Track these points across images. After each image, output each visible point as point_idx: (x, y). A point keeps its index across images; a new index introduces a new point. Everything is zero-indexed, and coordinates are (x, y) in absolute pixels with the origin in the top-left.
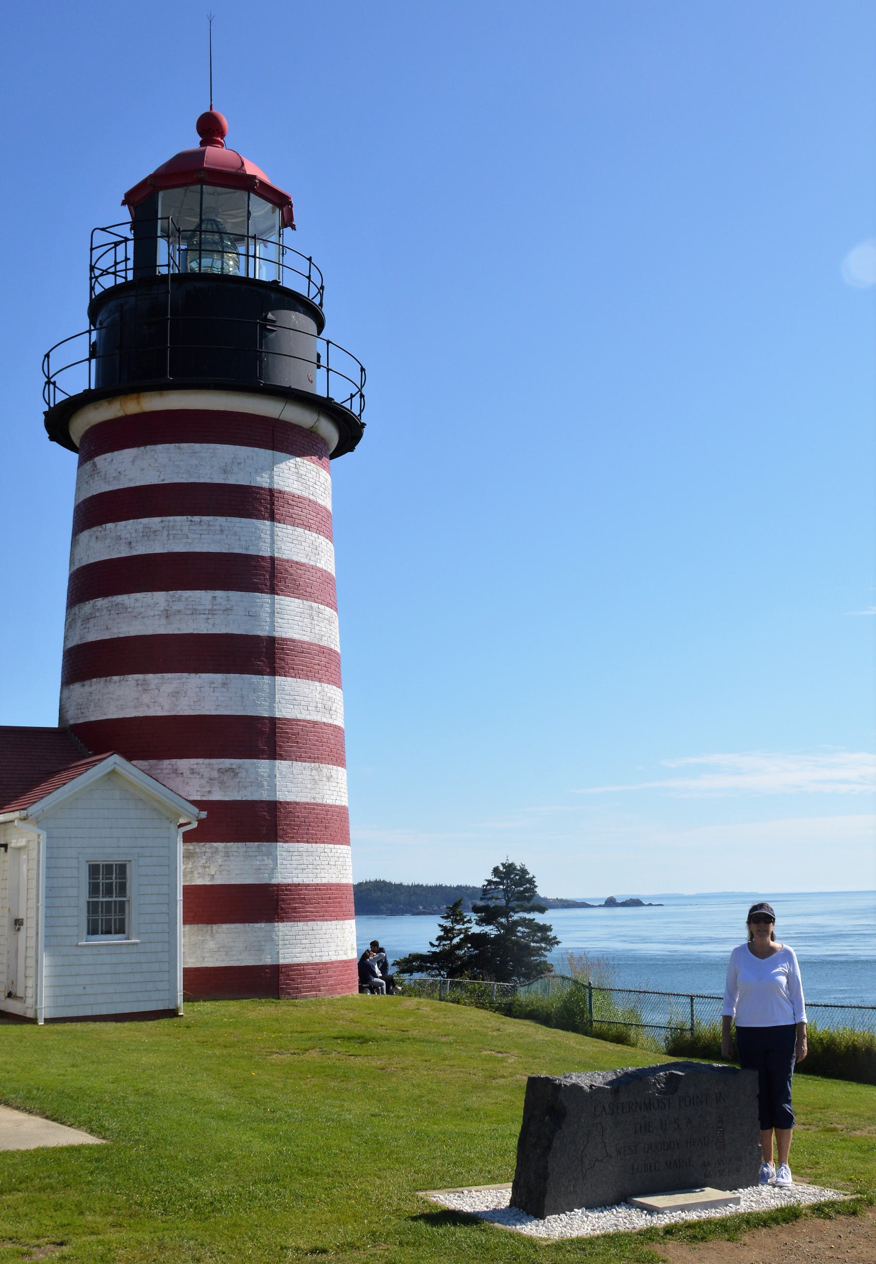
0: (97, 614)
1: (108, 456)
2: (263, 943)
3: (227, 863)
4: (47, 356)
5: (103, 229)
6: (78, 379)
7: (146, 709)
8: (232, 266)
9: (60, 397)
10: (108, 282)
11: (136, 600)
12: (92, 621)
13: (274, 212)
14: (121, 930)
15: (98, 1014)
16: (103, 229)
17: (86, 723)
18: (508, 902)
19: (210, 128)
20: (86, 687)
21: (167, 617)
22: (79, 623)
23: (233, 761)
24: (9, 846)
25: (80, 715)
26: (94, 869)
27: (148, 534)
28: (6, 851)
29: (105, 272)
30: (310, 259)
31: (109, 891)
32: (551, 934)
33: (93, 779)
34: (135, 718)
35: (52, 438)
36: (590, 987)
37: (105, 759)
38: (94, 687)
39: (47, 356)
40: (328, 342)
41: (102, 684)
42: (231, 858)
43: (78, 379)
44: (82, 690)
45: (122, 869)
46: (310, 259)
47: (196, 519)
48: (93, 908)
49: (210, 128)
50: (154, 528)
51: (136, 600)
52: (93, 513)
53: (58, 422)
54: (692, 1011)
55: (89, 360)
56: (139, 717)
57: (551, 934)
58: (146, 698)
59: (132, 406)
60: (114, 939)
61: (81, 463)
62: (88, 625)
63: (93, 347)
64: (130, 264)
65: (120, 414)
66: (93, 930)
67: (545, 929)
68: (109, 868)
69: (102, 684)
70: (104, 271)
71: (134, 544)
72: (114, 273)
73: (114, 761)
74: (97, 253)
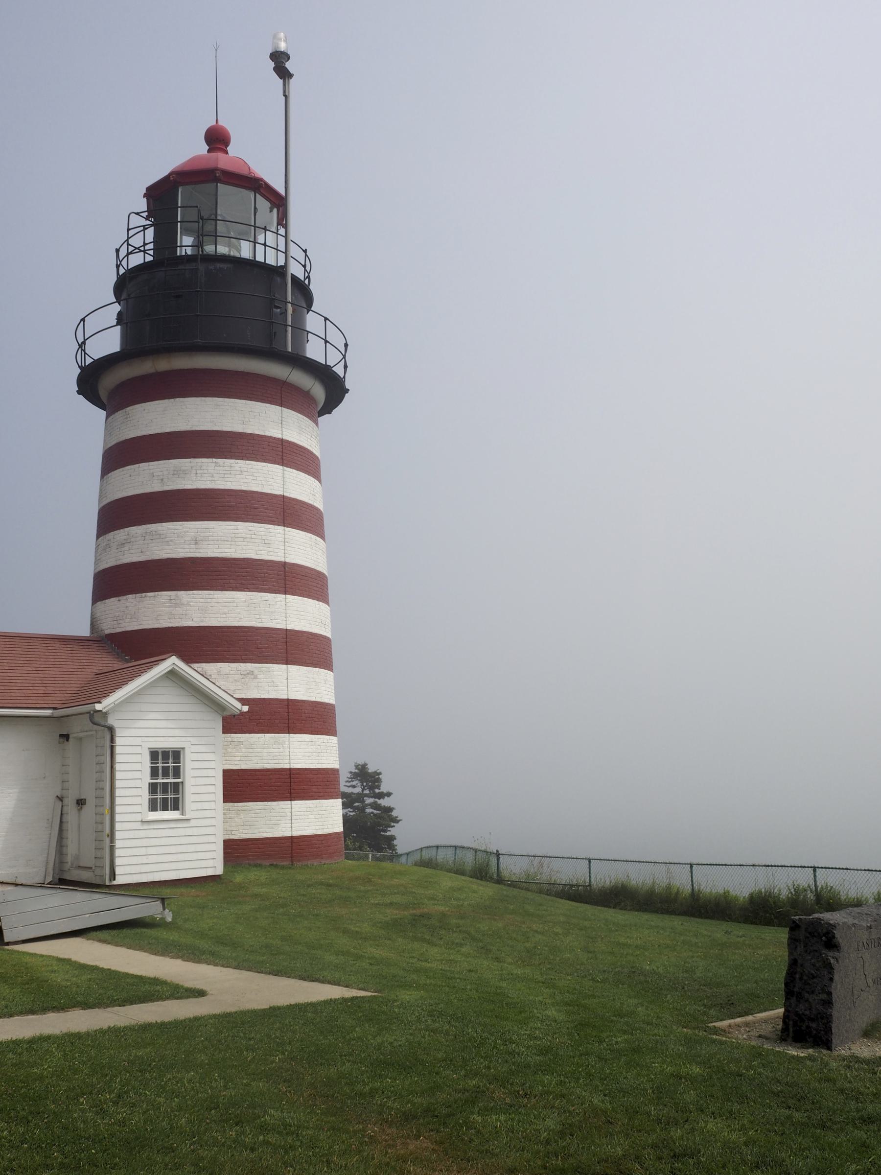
0: (133, 540)
1: (131, 408)
4: (83, 320)
5: (137, 214)
6: (108, 342)
8: (245, 251)
9: (89, 361)
10: (136, 260)
12: (127, 547)
13: (271, 211)
14: (176, 808)
16: (137, 214)
17: (122, 632)
18: (363, 790)
19: (217, 139)
20: (122, 602)
24: (71, 736)
25: (116, 626)
26: (154, 755)
27: (177, 472)
28: (68, 740)
29: (138, 250)
30: (305, 251)
31: (166, 773)
32: (394, 814)
36: (498, 855)
39: (83, 320)
40: (326, 319)
43: (108, 342)
46: (305, 251)
48: (153, 788)
49: (217, 139)
52: (120, 455)
53: (92, 381)
54: (815, 876)
55: (85, 340)
57: (394, 814)
59: (164, 364)
61: (107, 417)
62: (123, 549)
63: (120, 314)
64: (151, 246)
65: (152, 371)
66: (153, 807)
67: (390, 809)
68: (166, 754)
69: (138, 599)
70: (136, 248)
71: (165, 480)
72: (145, 251)
73: (173, 662)
74: (131, 233)
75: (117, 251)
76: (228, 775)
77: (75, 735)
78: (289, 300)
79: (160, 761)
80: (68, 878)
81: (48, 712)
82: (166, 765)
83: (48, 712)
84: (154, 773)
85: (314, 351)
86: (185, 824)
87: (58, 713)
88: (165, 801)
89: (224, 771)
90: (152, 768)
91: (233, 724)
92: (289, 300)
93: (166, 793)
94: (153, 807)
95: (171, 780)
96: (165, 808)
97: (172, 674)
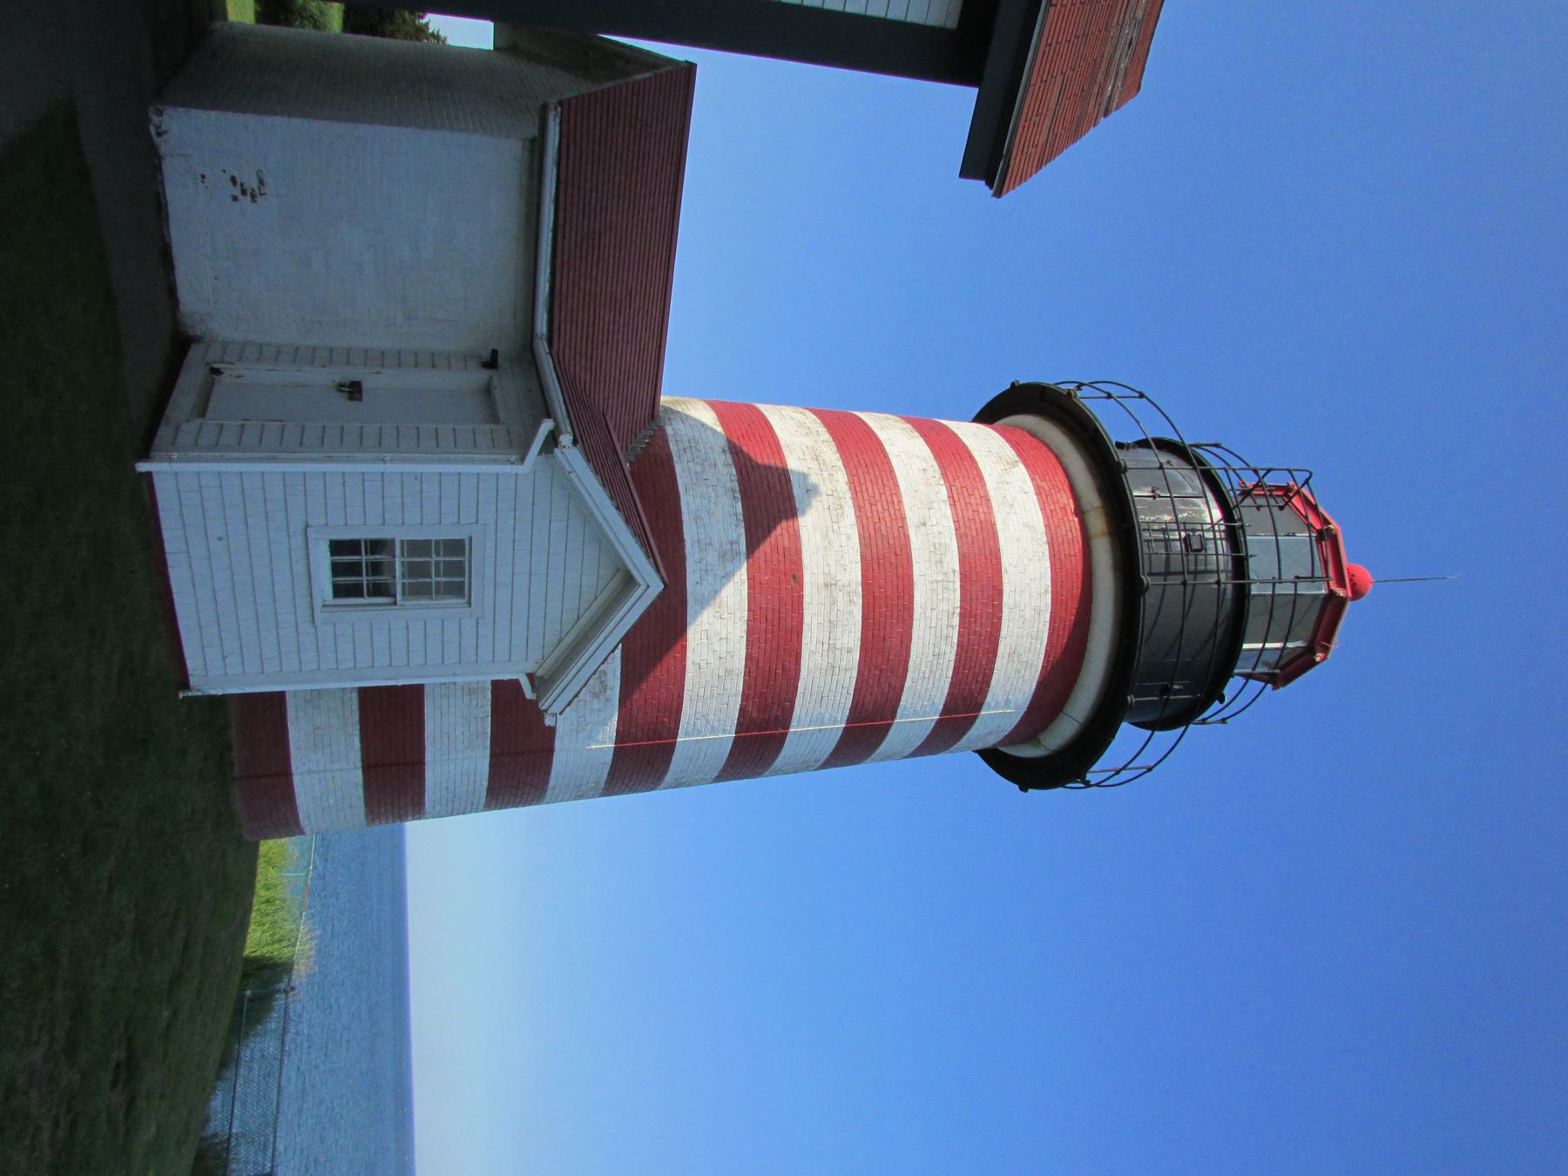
2: (327, 751)
3: (459, 693)
4: (1142, 396)
7: (697, 557)
11: (849, 538)
14: (339, 591)
15: (169, 563)
21: (826, 585)
22: (808, 441)
23: (617, 690)
26: (456, 547)
31: (413, 570)
33: (624, 556)
34: (681, 540)
35: (1014, 387)
37: (658, 570)
38: (724, 471)
39: (1142, 396)
41: (729, 485)
42: (466, 698)
44: (718, 449)
45: (457, 590)
47: (956, 621)
50: (946, 560)
51: (849, 538)
56: (683, 547)
58: (712, 557)
60: (324, 581)
66: (337, 547)
68: (458, 569)
75: (1217, 446)
76: (414, 695)
77: (495, 380)
78: (1268, 645)
79: (441, 559)
80: (1080, 567)
81: (542, 326)
82: (443, 569)
83: (542, 326)
84: (418, 547)
85: (1128, 736)
86: (304, 613)
87: (542, 347)
88: (354, 569)
89: (278, 700)
90: (428, 542)
91: (506, 697)
92: (1268, 645)
93: (360, 569)
94: (337, 547)
95: (399, 582)
96: (337, 569)
97: (628, 582)
